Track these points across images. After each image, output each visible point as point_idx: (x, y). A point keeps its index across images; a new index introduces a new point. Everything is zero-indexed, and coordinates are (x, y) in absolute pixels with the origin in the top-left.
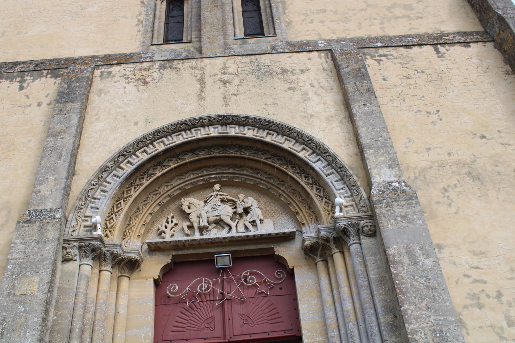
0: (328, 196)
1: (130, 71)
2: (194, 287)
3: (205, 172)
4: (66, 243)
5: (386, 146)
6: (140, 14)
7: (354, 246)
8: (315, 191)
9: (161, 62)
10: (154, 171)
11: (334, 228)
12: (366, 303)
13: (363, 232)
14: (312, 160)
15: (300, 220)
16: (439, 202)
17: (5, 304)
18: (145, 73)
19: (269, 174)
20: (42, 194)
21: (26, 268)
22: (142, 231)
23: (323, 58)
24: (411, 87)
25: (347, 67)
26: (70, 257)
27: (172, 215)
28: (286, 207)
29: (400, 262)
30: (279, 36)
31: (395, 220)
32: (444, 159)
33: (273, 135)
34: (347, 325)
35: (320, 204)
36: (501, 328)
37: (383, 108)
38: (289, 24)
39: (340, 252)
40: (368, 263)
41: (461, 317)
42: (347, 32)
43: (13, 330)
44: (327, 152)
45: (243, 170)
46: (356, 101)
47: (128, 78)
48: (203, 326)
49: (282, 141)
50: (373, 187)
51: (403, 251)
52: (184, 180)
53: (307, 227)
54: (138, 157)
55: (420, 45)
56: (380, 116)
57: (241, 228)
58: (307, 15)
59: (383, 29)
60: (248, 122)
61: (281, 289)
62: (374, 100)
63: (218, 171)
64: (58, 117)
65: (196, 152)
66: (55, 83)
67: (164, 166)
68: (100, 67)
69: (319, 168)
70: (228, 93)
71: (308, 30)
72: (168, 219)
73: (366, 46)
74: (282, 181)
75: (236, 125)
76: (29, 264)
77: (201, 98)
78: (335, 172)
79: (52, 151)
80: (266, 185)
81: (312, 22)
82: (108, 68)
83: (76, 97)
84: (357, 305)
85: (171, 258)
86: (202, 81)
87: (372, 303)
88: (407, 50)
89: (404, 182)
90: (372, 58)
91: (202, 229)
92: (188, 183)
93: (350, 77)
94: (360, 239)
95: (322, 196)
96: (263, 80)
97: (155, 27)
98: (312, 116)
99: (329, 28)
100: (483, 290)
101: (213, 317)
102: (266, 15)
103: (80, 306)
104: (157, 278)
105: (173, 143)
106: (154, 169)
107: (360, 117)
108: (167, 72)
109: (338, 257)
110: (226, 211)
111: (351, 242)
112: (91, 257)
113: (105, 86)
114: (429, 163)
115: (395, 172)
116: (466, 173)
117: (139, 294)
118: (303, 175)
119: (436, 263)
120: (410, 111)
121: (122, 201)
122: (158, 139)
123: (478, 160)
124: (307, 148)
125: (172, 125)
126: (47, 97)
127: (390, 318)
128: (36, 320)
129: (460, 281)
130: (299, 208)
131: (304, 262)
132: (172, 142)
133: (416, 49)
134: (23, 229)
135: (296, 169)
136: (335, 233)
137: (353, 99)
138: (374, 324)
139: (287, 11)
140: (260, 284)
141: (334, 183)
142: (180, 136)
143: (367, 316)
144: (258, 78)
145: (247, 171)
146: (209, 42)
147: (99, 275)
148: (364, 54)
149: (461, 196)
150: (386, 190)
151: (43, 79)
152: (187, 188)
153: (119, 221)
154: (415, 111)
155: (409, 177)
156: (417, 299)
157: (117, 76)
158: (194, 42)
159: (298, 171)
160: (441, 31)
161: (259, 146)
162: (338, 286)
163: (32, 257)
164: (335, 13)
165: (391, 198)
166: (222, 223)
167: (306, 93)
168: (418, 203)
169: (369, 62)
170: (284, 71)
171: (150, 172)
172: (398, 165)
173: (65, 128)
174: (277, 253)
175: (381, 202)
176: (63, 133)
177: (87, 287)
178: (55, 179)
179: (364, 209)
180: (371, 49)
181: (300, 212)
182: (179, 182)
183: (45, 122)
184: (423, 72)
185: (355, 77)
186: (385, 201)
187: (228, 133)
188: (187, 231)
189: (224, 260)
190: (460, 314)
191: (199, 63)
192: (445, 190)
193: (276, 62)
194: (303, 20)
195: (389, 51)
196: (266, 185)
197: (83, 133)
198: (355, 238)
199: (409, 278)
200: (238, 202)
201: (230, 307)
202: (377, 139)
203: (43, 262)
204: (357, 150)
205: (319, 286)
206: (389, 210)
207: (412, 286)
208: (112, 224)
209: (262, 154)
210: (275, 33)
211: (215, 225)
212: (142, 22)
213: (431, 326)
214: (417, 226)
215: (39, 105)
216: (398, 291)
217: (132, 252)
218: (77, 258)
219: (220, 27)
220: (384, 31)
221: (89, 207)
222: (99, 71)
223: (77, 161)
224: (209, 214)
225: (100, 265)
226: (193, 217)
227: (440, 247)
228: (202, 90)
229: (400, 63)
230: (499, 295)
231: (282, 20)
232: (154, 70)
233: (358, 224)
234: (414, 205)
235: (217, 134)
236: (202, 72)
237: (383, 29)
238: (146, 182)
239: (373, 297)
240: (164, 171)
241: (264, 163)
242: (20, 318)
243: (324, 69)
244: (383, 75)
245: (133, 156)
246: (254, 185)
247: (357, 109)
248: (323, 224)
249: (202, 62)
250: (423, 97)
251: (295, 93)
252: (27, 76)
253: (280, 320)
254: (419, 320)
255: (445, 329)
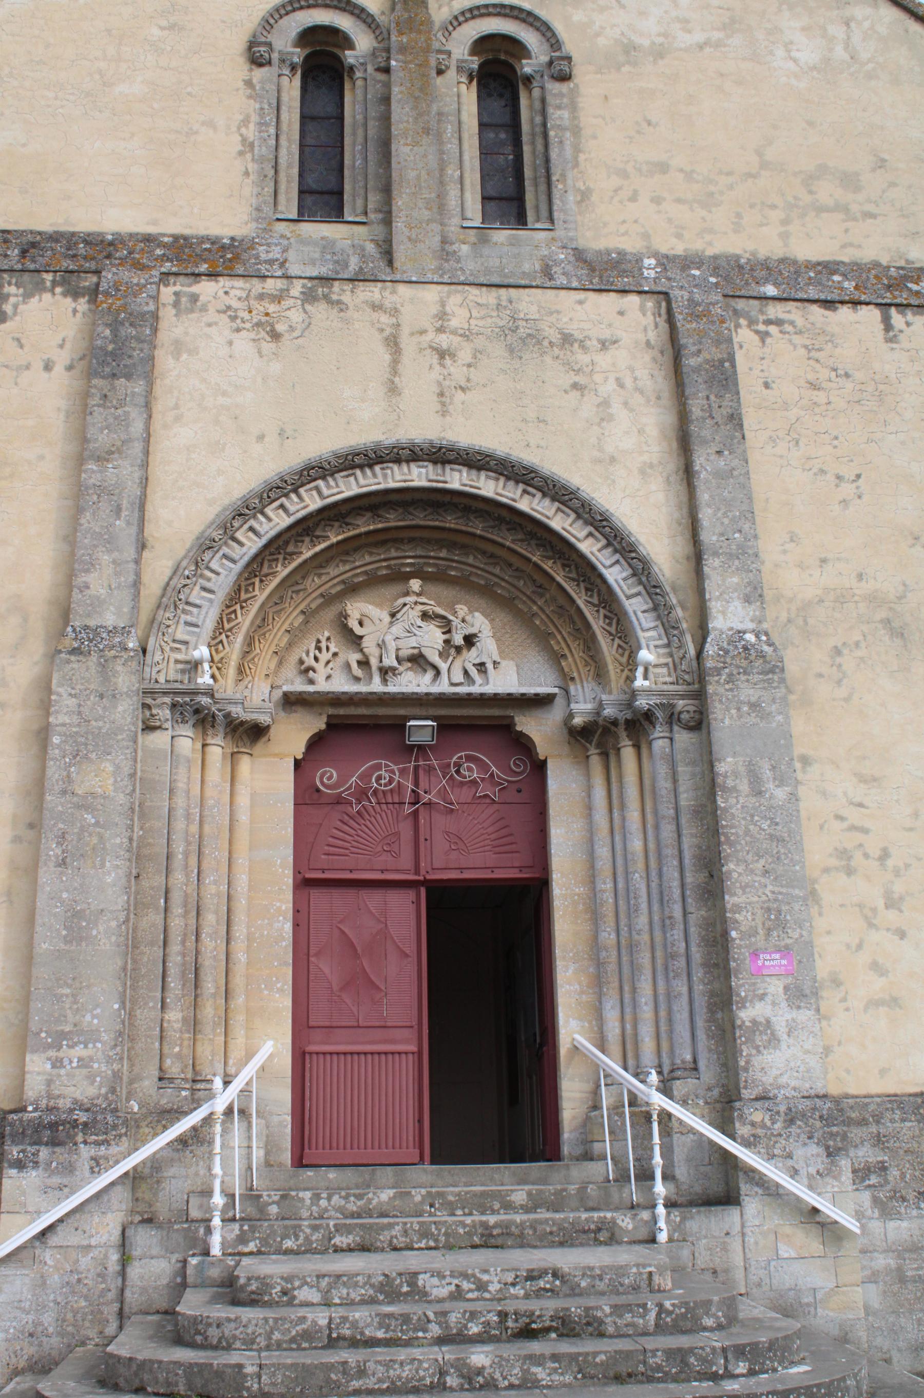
0: (628, 644)
1: (239, 299)
2: (366, 777)
3: (393, 550)
4: (149, 695)
5: (745, 555)
6: (246, 122)
7: (660, 742)
8: (601, 622)
9: (306, 281)
10: (296, 546)
11: (629, 704)
12: (667, 846)
13: (679, 720)
14: (604, 561)
15: (566, 670)
16: (820, 675)
17: (60, 808)
18: (272, 308)
19: (517, 570)
20: (92, 592)
21: (86, 744)
22: (273, 666)
23: (649, 313)
24: (817, 410)
25: (698, 323)
26: (158, 724)
27: (327, 634)
28: (543, 639)
29: (734, 789)
30: (560, 233)
31: (739, 709)
32: (848, 586)
33: (534, 496)
34: (630, 876)
35: (607, 648)
36: (874, 910)
37: (754, 457)
38: (585, 195)
39: (634, 746)
40: (681, 779)
41: (816, 886)
42: (708, 237)
43: (82, 855)
44: (635, 551)
45: (467, 555)
46: (705, 442)
47: (236, 317)
48: (379, 848)
49: (550, 513)
50: (709, 640)
51: (742, 769)
52: (352, 566)
53: (579, 687)
54: (269, 519)
55: (856, 303)
56: (745, 487)
57: (458, 677)
58: (624, 174)
59: (785, 236)
60: (488, 463)
61: (519, 791)
62: (739, 443)
63: (419, 552)
64: (101, 414)
65: (381, 512)
66: (75, 311)
67: (318, 537)
68: (172, 279)
69: (616, 581)
70: (447, 383)
71: (624, 222)
72: (319, 641)
73: (743, 293)
74: (540, 587)
75: (464, 465)
76: (90, 737)
77: (393, 390)
78: (644, 592)
79: (99, 496)
80: (509, 592)
81: (633, 198)
82: (190, 285)
83: (134, 364)
84: (652, 846)
85: (325, 720)
86: (393, 343)
87: (676, 847)
88: (827, 313)
89: (766, 634)
90: (749, 326)
91: (385, 672)
92: (359, 571)
93: (700, 380)
94: (671, 731)
95: (614, 632)
96: (521, 358)
97: (280, 161)
98: (613, 460)
99: (670, 221)
100: (861, 845)
101: (397, 834)
102: (534, 152)
103: (180, 812)
104: (300, 757)
105: (338, 493)
106: (297, 541)
107: (707, 481)
108: (319, 311)
109: (628, 753)
110: (431, 638)
111: (656, 735)
112: (191, 723)
113: (186, 333)
114: (819, 592)
115: (753, 610)
116: (881, 621)
117: (267, 784)
118: (582, 585)
119: (794, 797)
120: (804, 470)
121: (238, 607)
122: (309, 483)
123: (909, 595)
124: (597, 534)
125: (337, 456)
126: (61, 346)
127: (702, 877)
128: (118, 841)
129: (826, 826)
130: (568, 646)
131: (566, 749)
132: (335, 491)
133: (845, 311)
134: (68, 667)
135: (570, 572)
136: (629, 712)
137: (699, 436)
138: (676, 884)
139: (582, 157)
140: (483, 779)
141: (640, 615)
142: (352, 479)
143: (665, 869)
144: (511, 350)
145: (475, 557)
146: (410, 239)
147: (203, 753)
148: (735, 312)
149: (862, 666)
150: (731, 648)
151: (47, 296)
152: (356, 580)
153: (234, 650)
154: (815, 470)
155: (777, 618)
156: (751, 855)
157: (212, 310)
158: (373, 223)
159: (574, 575)
160: (907, 261)
161: (504, 513)
162: (623, 806)
163: (93, 723)
164: (689, 176)
165: (738, 667)
166: (422, 662)
167: (606, 403)
168: (783, 680)
169: (744, 336)
170: (567, 339)
171: (291, 548)
172: (761, 596)
173: (119, 443)
174: (518, 728)
175: (718, 672)
176: (116, 456)
177: (189, 778)
178: (114, 562)
179: (686, 677)
180: (752, 302)
181: (569, 655)
182: (342, 569)
183: (67, 412)
184: (847, 375)
185: (710, 383)
186: (727, 670)
187: (446, 482)
188: (357, 671)
189: (421, 728)
190: (814, 881)
191: (386, 294)
192: (837, 651)
193: (551, 313)
194: (616, 191)
195: (789, 312)
196: (509, 592)
197: (151, 449)
198: (666, 727)
199: (744, 819)
200: (456, 622)
201: (428, 818)
202: (730, 536)
203: (116, 735)
204: (689, 549)
205: (589, 796)
206: (731, 690)
207: (747, 832)
208: (221, 655)
209: (508, 530)
210: (551, 220)
211: (409, 665)
212: (252, 145)
213: (764, 902)
214: (774, 725)
215: (48, 367)
216: (722, 839)
217: (259, 710)
218: (168, 725)
219: (433, 195)
220: (786, 245)
221: (182, 621)
222: (171, 289)
223: (146, 518)
224: (401, 643)
225: (205, 734)
226: (369, 644)
227: (806, 761)
228: (395, 362)
229: (806, 347)
230: (885, 855)
231: (570, 182)
232: (292, 301)
233: (673, 706)
234: (775, 684)
235: (424, 483)
236: (394, 320)
237: (785, 236)
238: (283, 571)
239: (679, 836)
240: (318, 548)
241: (509, 549)
242: (90, 835)
243: (648, 343)
244: (766, 374)
245: (260, 516)
246: (486, 586)
247: (703, 460)
248: (610, 693)
249: (394, 292)
250: (836, 438)
251: (585, 399)
252: (10, 284)
253: (513, 847)
254: (748, 890)
255: (784, 908)
